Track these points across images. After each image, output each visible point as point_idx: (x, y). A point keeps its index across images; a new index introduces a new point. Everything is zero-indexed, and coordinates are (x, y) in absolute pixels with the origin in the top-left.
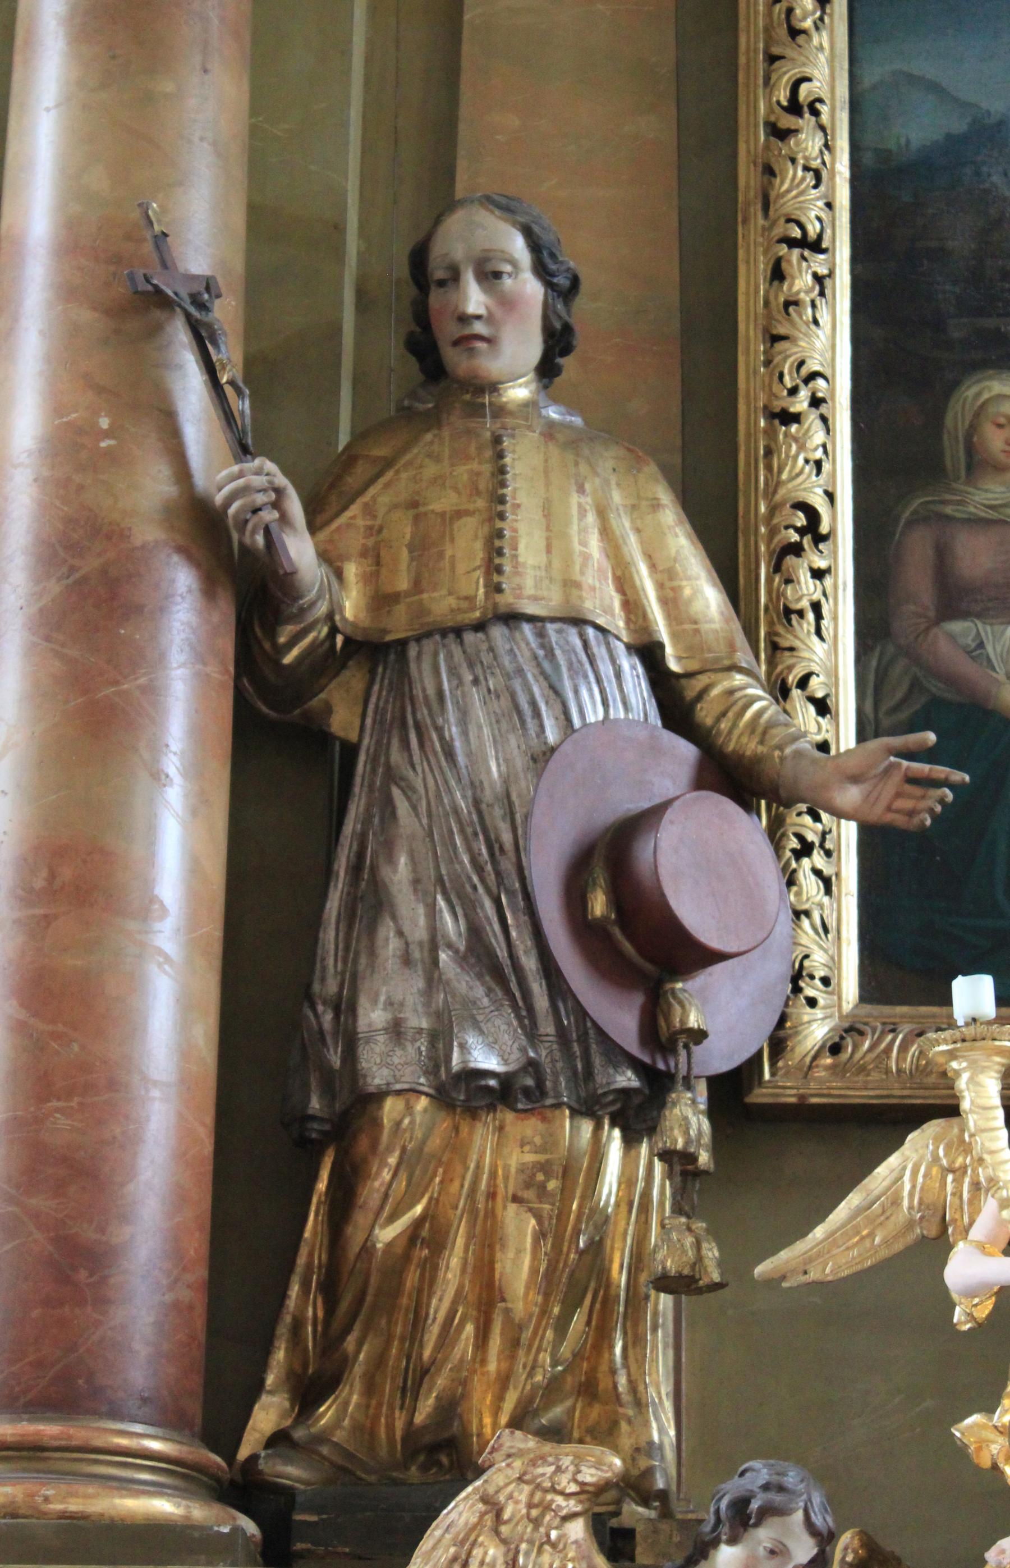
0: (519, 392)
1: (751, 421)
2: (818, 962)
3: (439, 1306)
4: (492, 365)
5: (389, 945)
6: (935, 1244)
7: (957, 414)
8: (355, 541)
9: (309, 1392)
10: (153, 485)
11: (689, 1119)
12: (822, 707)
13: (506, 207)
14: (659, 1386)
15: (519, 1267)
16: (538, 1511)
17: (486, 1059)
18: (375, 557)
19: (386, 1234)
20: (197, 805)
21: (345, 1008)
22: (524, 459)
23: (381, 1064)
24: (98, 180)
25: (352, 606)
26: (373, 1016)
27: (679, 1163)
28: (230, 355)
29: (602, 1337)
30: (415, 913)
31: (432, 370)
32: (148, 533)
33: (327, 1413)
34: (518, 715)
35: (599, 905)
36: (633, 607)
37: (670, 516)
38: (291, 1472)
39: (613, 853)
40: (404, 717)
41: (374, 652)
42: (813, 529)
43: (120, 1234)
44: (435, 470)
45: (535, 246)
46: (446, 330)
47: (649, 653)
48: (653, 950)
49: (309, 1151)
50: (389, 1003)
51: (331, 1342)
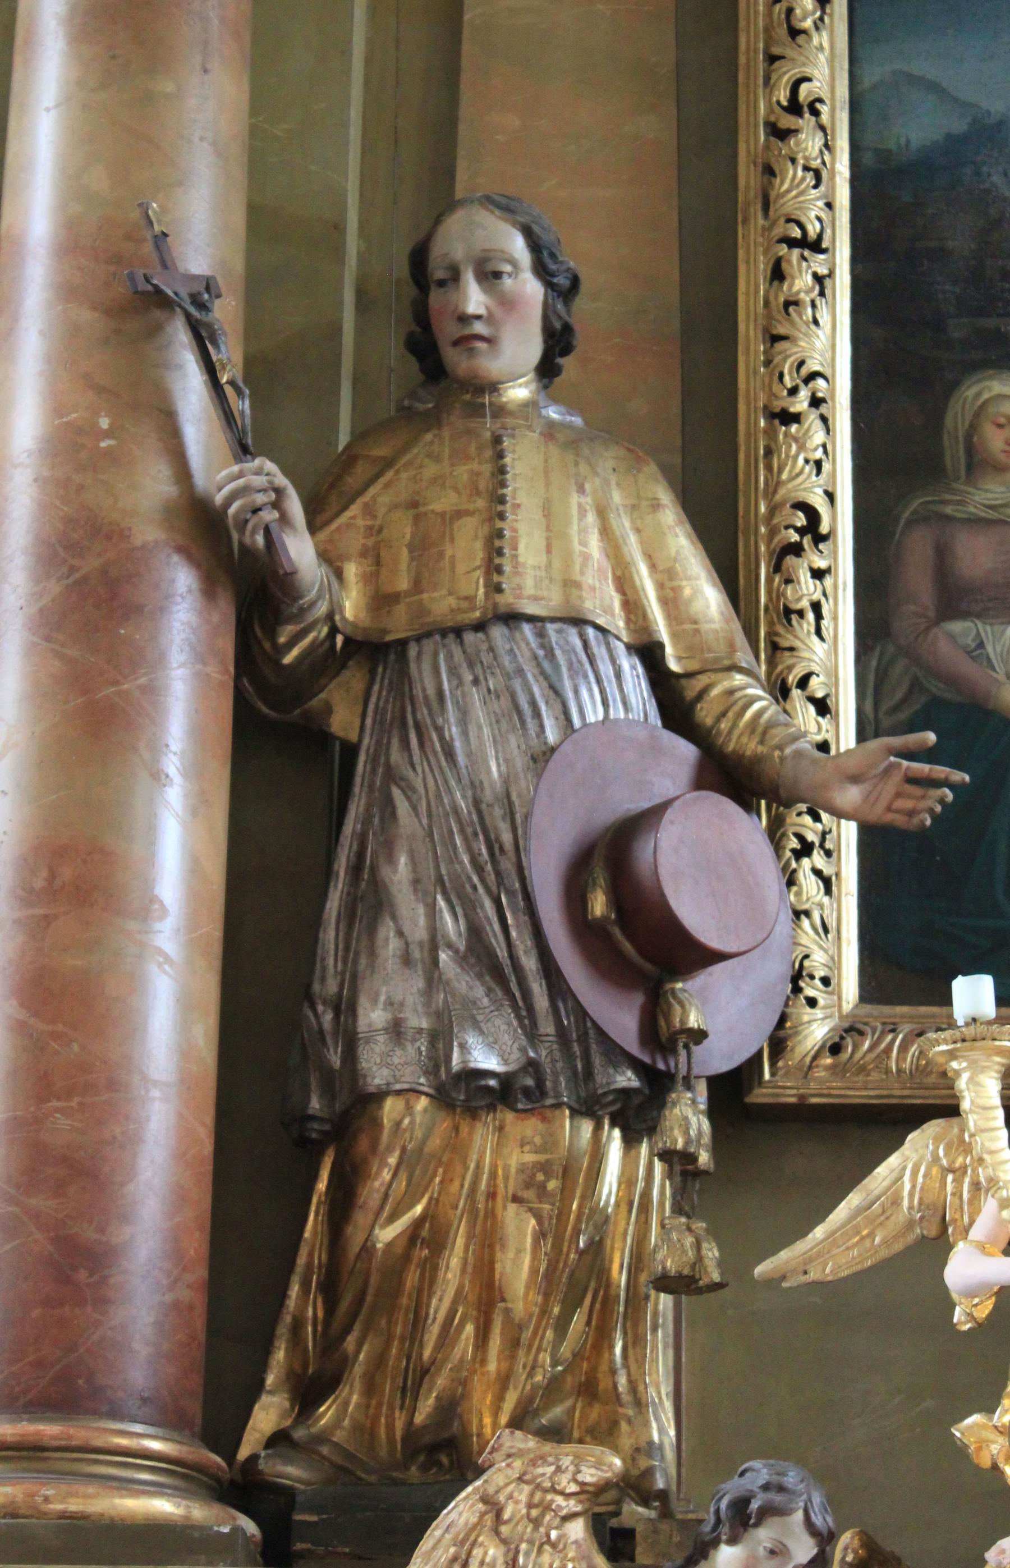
0: (519, 392)
1: (751, 421)
2: (818, 962)
3: (439, 1306)
4: (492, 365)
5: (389, 945)
6: (935, 1244)
7: (957, 414)
8: (355, 541)
9: (309, 1392)
10: (153, 485)
11: (689, 1119)
12: (822, 707)
13: (506, 207)
14: (659, 1386)
15: (519, 1267)
16: (538, 1511)
17: (486, 1059)
18: (375, 557)
19: (386, 1234)
20: (197, 805)
21: (345, 1008)
22: (524, 459)
23: (381, 1064)
24: (98, 180)
25: (352, 606)
26: (373, 1016)
27: (679, 1163)
28: (230, 355)
29: (602, 1337)
30: (415, 913)
31: (432, 370)
32: (148, 533)
33: (327, 1413)
34: (518, 715)
35: (599, 905)
36: (633, 607)
37: (670, 516)
38: (291, 1472)
39: (613, 853)
40: (404, 717)
41: (374, 652)
42: (813, 529)
43: (120, 1234)
44: (435, 470)
45: (535, 246)
46: (446, 330)
47: (649, 653)
48: (653, 950)
49: (309, 1151)
50: (389, 1003)
51: (331, 1342)
